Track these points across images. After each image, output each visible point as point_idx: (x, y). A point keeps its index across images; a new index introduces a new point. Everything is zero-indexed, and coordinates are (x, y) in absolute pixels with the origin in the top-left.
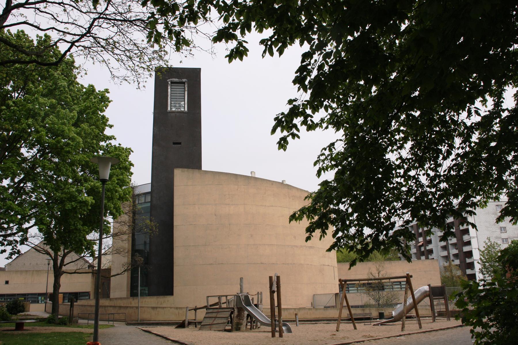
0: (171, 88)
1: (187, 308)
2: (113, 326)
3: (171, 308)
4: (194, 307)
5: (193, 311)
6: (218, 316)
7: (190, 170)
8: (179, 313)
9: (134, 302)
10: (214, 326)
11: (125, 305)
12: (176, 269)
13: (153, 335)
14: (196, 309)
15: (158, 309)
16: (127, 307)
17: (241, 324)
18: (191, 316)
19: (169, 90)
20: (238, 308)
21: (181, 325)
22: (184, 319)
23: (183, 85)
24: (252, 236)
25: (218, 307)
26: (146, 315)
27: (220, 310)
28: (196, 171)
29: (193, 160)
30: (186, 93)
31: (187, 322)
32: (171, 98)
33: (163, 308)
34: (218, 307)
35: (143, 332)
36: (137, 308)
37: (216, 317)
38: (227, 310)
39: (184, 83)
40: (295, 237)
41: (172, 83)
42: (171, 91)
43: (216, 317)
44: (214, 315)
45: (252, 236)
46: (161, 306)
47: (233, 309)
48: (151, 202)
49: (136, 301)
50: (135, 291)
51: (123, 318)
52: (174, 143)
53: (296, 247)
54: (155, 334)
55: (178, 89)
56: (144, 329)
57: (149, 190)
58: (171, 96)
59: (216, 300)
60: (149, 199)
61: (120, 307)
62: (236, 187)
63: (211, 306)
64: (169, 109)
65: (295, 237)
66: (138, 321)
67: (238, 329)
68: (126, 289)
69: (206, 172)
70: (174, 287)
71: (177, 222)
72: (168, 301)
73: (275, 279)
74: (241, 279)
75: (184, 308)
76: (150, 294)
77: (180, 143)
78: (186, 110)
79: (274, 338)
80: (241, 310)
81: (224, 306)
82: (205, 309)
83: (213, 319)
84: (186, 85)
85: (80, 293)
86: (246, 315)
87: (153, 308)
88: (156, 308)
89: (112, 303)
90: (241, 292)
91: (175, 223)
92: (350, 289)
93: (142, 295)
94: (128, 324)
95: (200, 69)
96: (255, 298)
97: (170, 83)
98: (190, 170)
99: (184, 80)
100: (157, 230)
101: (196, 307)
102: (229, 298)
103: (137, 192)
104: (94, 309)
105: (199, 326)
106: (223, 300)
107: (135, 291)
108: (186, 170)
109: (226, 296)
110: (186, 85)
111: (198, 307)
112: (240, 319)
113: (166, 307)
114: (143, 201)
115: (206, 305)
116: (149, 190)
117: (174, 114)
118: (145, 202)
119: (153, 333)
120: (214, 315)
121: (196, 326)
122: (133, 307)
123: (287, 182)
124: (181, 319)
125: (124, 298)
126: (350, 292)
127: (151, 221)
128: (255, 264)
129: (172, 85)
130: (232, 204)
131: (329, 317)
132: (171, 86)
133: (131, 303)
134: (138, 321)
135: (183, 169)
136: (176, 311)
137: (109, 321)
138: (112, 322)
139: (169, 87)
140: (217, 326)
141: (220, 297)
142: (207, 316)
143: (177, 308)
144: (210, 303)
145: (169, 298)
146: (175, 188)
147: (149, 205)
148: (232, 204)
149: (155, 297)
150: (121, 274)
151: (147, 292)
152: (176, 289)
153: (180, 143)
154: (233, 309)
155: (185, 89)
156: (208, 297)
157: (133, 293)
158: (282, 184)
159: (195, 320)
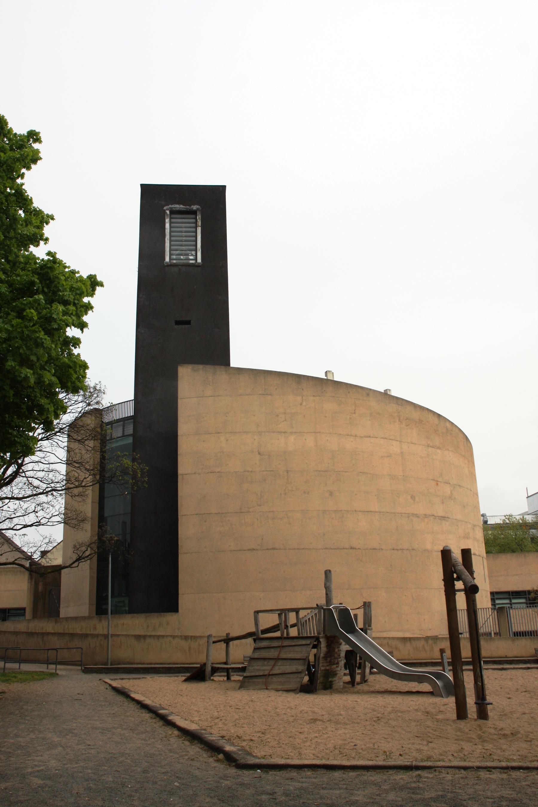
0: (171, 223)
1: (209, 636)
2: (54, 675)
3: (174, 637)
4: (223, 635)
5: (224, 645)
6: (283, 656)
7: (210, 368)
8: (190, 648)
9: (101, 626)
10: (275, 679)
11: (84, 632)
12: (183, 560)
13: (132, 706)
14: (227, 640)
15: (148, 640)
16: (85, 636)
17: (335, 674)
18: (217, 654)
19: (167, 226)
20: (327, 638)
21: (198, 675)
22: (202, 659)
23: (193, 216)
24: (331, 494)
25: (278, 634)
26: (123, 653)
27: (286, 643)
28: (220, 371)
29: (214, 347)
30: (199, 230)
31: (208, 669)
32: (171, 241)
33: (159, 637)
34: (278, 634)
35: (111, 694)
36: (106, 636)
37: (277, 659)
38: (304, 642)
39: (194, 213)
40: (413, 497)
41: (172, 212)
42: (171, 227)
43: (277, 659)
44: (273, 653)
45: (331, 494)
46: (153, 634)
47: (317, 639)
48: (134, 435)
49: (104, 623)
50: (104, 607)
51: (79, 658)
52: (178, 323)
53: (417, 516)
54: (138, 702)
55: (184, 224)
56: (115, 684)
57: (131, 413)
58: (171, 236)
59: (272, 620)
60: (130, 430)
61: (73, 635)
62: (299, 398)
63: (265, 631)
64: (167, 259)
65: (413, 497)
66: (106, 664)
67: (328, 686)
68: (87, 601)
69: (240, 371)
70: (180, 596)
71: (185, 466)
72: (168, 623)
73: (457, 556)
74: (328, 573)
75: (200, 637)
76: (134, 610)
77: (188, 323)
78: (199, 260)
79: (462, 724)
80: (333, 641)
81: (293, 632)
82: (250, 640)
83: (272, 662)
84: (199, 217)
85: (10, 609)
86: (343, 654)
87: (138, 637)
88: (145, 637)
89: (59, 628)
90: (329, 600)
91: (181, 470)
92: (514, 601)
93: (117, 612)
94: (87, 671)
95: (224, 187)
96: (360, 613)
97: (168, 212)
98: (208, 367)
99: (195, 207)
100: (146, 479)
101: (228, 634)
102: (302, 613)
103: (107, 419)
104: (446, 645)
105: (236, 677)
106: (292, 618)
107: (104, 607)
108: (201, 367)
109: (297, 611)
110: (199, 217)
111: (233, 634)
112: (331, 663)
113: (163, 636)
114: (120, 434)
115: (253, 630)
116: (131, 413)
117: (176, 269)
118: (123, 436)
119: (133, 699)
120: (273, 653)
121: (229, 678)
122: (97, 636)
123: (393, 393)
124: (198, 659)
125: (83, 618)
126: (513, 606)
127: (134, 460)
128: (338, 549)
129: (173, 216)
130: (291, 433)
131: (495, 655)
132: (171, 218)
133: (95, 628)
134: (106, 664)
135: (196, 367)
136: (183, 643)
137: (48, 662)
138: (54, 666)
139: (167, 220)
140: (281, 679)
141: (283, 612)
142: (256, 655)
143: (186, 638)
144: (262, 627)
145: (170, 618)
146: (179, 401)
147: (130, 440)
148: (291, 433)
149: (143, 615)
150: (70, 566)
151: (127, 609)
152: (184, 600)
153: (188, 323)
154: (317, 639)
155: (196, 223)
156: (257, 612)
157: (100, 609)
158: (386, 394)
159: (226, 663)
